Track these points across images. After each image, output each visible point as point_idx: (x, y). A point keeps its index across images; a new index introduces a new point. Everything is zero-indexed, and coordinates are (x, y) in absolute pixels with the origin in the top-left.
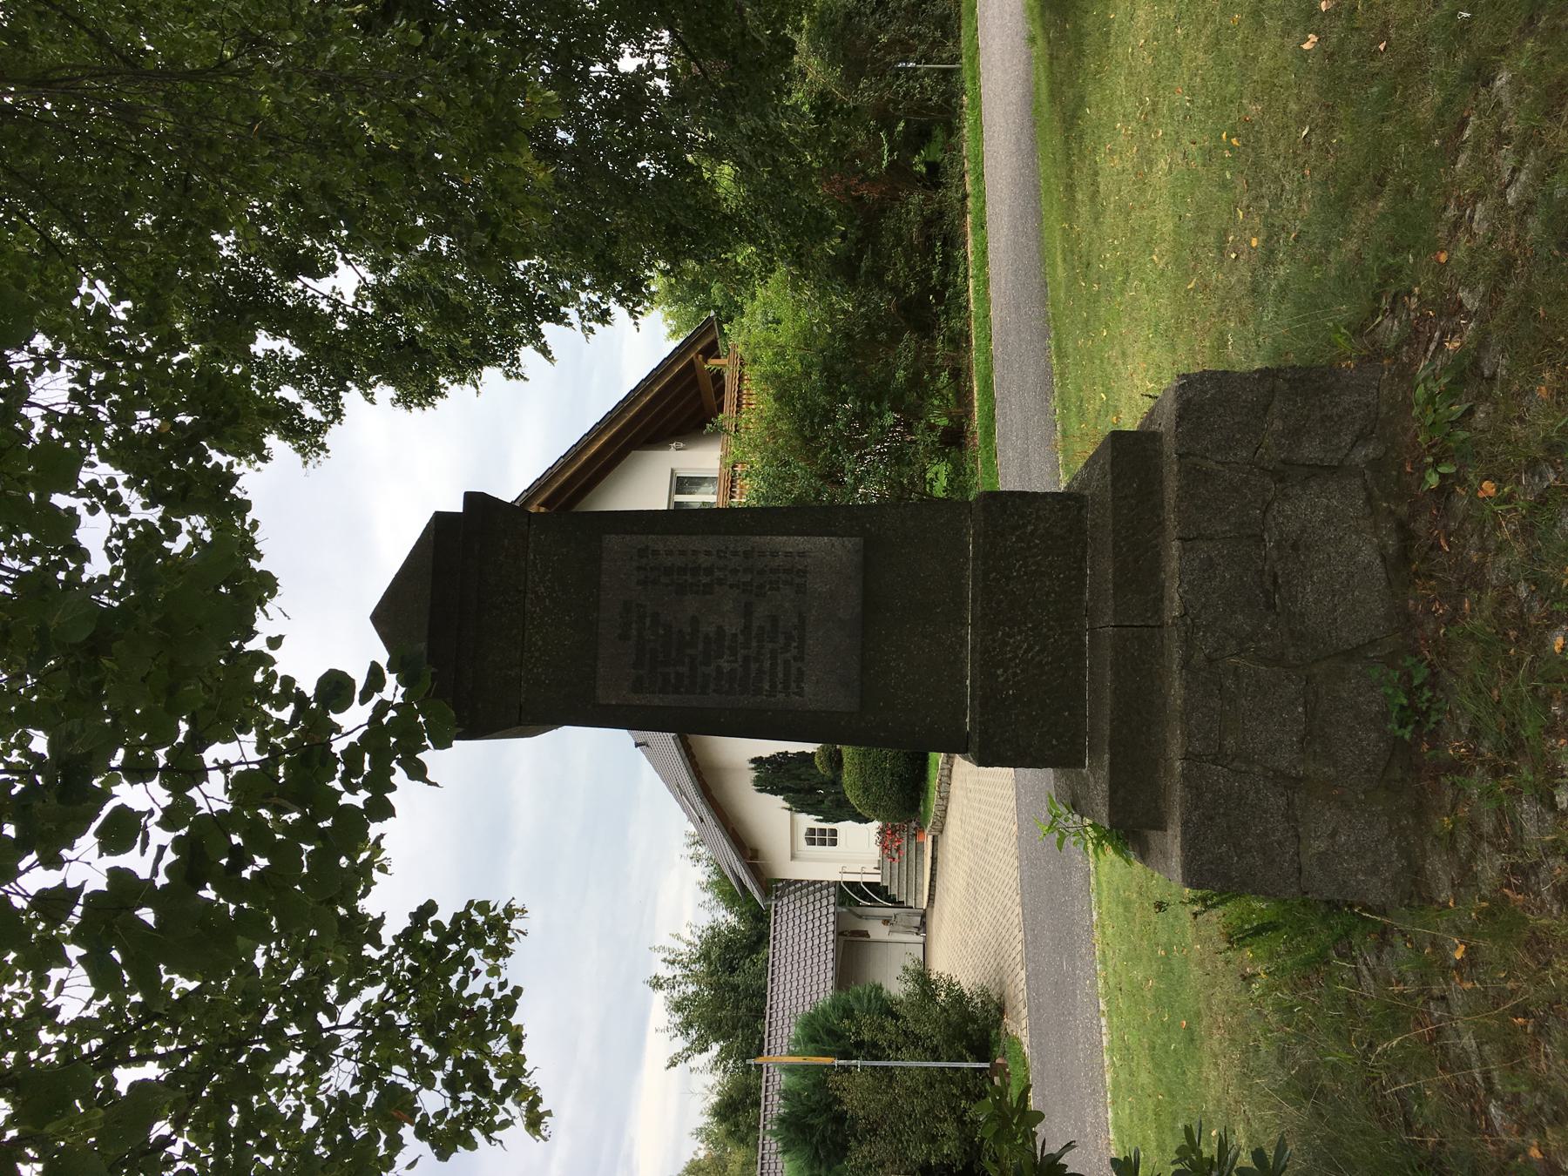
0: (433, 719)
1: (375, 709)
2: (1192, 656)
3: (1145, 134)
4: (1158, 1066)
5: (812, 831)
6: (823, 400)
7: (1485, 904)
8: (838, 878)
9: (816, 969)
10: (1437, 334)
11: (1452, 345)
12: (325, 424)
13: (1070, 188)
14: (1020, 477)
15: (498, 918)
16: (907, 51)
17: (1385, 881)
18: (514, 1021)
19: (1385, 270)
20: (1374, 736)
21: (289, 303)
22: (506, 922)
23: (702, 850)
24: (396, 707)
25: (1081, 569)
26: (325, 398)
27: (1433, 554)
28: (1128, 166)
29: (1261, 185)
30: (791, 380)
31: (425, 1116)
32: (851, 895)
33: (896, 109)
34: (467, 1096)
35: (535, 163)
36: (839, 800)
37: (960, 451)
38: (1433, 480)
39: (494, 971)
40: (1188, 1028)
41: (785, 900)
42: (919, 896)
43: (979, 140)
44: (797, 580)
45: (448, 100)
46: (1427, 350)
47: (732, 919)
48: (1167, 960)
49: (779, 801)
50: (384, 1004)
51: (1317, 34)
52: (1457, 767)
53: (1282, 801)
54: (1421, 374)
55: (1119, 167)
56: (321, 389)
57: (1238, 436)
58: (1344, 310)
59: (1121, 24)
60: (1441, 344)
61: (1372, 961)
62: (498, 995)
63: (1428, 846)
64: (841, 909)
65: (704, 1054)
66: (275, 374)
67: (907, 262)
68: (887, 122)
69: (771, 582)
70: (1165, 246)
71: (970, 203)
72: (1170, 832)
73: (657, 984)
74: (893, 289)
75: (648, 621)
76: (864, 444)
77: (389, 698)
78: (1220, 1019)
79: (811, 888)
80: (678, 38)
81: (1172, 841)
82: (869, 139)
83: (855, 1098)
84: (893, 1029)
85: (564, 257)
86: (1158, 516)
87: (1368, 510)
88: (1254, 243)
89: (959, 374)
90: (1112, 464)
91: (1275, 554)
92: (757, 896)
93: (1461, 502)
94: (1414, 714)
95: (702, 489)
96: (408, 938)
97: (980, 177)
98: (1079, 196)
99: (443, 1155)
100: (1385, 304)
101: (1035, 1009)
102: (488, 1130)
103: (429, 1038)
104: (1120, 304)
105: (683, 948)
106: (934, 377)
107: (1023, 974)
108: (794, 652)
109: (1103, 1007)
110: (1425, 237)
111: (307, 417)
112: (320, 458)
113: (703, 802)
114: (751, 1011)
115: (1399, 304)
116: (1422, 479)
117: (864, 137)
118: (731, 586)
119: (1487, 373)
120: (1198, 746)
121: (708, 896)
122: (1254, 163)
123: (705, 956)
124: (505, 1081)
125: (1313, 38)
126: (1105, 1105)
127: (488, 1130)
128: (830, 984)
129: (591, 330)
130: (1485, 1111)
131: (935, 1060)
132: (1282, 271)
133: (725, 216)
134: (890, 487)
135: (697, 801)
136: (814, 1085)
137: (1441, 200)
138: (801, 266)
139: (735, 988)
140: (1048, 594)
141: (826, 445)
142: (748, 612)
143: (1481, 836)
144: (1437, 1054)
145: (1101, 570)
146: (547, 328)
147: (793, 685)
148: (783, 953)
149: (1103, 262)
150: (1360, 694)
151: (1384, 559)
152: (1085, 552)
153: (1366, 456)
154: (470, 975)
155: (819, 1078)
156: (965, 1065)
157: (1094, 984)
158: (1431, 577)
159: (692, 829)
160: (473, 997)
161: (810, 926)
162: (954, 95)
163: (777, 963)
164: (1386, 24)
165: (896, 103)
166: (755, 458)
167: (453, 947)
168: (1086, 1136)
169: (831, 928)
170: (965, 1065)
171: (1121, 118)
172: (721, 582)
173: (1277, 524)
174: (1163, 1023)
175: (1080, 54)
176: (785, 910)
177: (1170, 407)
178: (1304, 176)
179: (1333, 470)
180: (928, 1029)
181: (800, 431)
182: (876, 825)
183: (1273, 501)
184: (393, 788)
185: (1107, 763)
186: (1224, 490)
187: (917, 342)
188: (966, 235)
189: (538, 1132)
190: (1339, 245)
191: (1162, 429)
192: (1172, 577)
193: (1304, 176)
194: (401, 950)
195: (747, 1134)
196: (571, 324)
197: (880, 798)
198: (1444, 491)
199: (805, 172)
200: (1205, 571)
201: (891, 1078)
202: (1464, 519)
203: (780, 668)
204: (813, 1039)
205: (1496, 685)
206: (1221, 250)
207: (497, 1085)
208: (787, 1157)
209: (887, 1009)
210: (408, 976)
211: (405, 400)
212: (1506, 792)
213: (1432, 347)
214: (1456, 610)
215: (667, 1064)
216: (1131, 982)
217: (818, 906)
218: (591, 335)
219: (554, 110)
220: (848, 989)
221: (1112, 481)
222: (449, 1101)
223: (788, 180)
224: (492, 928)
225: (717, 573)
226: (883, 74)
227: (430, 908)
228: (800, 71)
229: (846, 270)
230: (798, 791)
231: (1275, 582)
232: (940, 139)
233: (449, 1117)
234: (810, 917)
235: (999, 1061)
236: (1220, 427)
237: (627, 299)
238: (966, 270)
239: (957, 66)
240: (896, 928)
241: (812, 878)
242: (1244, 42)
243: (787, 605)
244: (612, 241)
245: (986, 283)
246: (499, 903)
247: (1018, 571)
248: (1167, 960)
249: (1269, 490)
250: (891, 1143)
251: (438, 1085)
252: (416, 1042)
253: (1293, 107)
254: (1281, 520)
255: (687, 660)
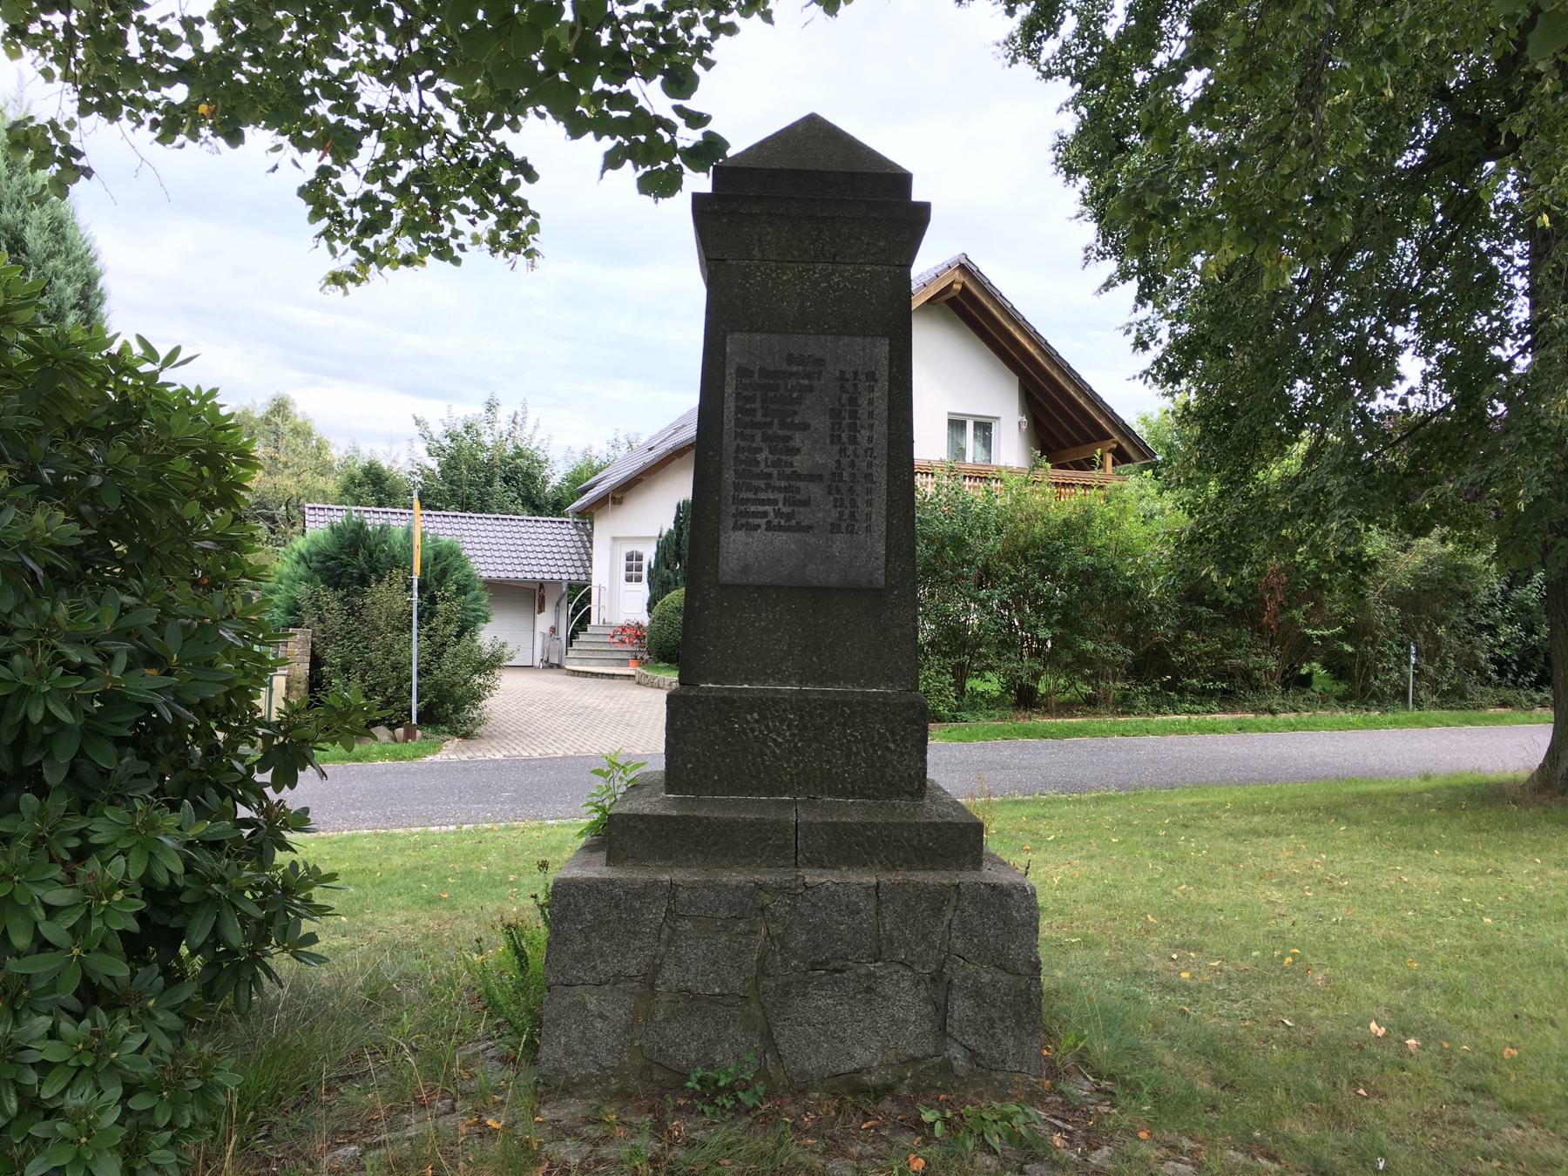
0: (665, 176)
1: (668, 121)
2: (766, 892)
3: (1311, 881)
4: (407, 872)
5: (640, 558)
6: (1064, 567)
7: (535, 1146)
8: (595, 583)
9: (507, 561)
10: (1070, 1127)
11: (1057, 1139)
12: (1037, 63)
13: (1266, 811)
14: (982, 761)
15: (525, 243)
16: (1429, 655)
17: (560, 1062)
18: (430, 259)
19: (1139, 1086)
20: (693, 1056)
21: (1164, 23)
22: (523, 251)
23: (624, 450)
24: (673, 142)
25: (853, 794)
26: (1063, 62)
27: (859, 1114)
28: (1281, 864)
29: (1242, 982)
30: (1084, 535)
31: (337, 175)
32: (579, 597)
33: (1366, 644)
34: (358, 214)
35: (1225, 262)
36: (669, 583)
37: (1013, 705)
38: (928, 1117)
39: (476, 239)
40: (441, 899)
41: (574, 532)
42: (577, 662)
43: (1331, 727)
44: (844, 525)
45: (1289, 177)
46: (1055, 1117)
47: (555, 481)
48: (504, 882)
49: (669, 524)
50: (442, 134)
51: (1385, 1036)
52: (659, 1128)
53: (632, 971)
54: (1031, 1111)
55: (1281, 856)
56: (1073, 57)
57: (976, 941)
58: (1101, 1048)
59: (1428, 860)
60: (1060, 1129)
61: (490, 1053)
62: (453, 243)
63: (590, 1102)
64: (565, 585)
65: (426, 453)
66: (1088, 11)
67: (1206, 653)
68: (1351, 634)
69: (842, 499)
70: (1194, 896)
71: (1267, 717)
72: (605, 869)
73: (491, 407)
74: (1178, 638)
75: (806, 382)
76: (1020, 610)
77: (679, 133)
78: (448, 926)
79: (585, 557)
80: (1432, 417)
81: (598, 870)
82: (1335, 616)
83: (387, 598)
84: (447, 632)
85: (1201, 302)
86: (901, 866)
87: (904, 1058)
88: (1185, 975)
89: (1091, 704)
90: (950, 823)
91: (863, 971)
92: (578, 503)
93: (904, 1139)
94: (710, 1092)
95: (980, 448)
96: (503, 156)
97: (1292, 727)
98: (1257, 819)
99: (303, 192)
100: (1104, 1084)
101: (466, 767)
102: (327, 234)
103: (413, 177)
104: (1141, 854)
105: (528, 431)
106: (1087, 680)
107: (499, 756)
108: (775, 522)
109: (465, 827)
110: (1165, 1121)
111: (1044, 44)
112: (1003, 59)
113: (667, 450)
114: (468, 498)
115: (1103, 1096)
116: (930, 1107)
117: (1337, 611)
118: (838, 462)
119: (1027, 1167)
120: (684, 895)
121: (579, 457)
122: (1264, 977)
123: (519, 454)
124: (372, 250)
125: (1381, 1032)
126: (375, 828)
127: (327, 234)
128: (494, 575)
129: (1128, 332)
130: (351, 1142)
131: (418, 672)
132: (1152, 999)
133: (1247, 468)
134: (975, 635)
135: (669, 445)
136: (394, 557)
137: (1200, 1136)
138: (1190, 542)
139: (489, 482)
140: (829, 762)
141: (1018, 571)
142: (814, 478)
143: (597, 1145)
144: (404, 1103)
145: (851, 811)
146: (1133, 286)
147: (743, 521)
148: (523, 530)
149: (1187, 840)
150: (731, 1045)
151: (857, 1071)
152: (869, 798)
153: (956, 1058)
154: (471, 217)
155: (400, 562)
156: (414, 700)
157: (487, 820)
158: (838, 1111)
159: (644, 439)
160: (450, 219)
161: (549, 556)
162: (1380, 703)
163: (513, 523)
164: (1384, 1096)
165: (1372, 644)
166: (1003, 501)
167: (497, 199)
168: (347, 810)
169: (547, 576)
170: (414, 700)
171: (1331, 858)
172: (842, 451)
173: (891, 974)
174: (446, 877)
175: (1403, 822)
176: (564, 532)
177: (1005, 878)
178: (1244, 1020)
179: (943, 1027)
180: (448, 666)
181: (1034, 545)
182: (645, 619)
183: (913, 970)
184: (598, 138)
185: (669, 813)
186: (924, 926)
187: (1123, 662)
188: (1233, 712)
189: (328, 283)
190: (1171, 1048)
191: (985, 871)
192: (842, 876)
193: (1244, 1020)
194: (493, 149)
195: (352, 495)
196: (1135, 311)
197: (671, 624)
198: (919, 1126)
199: (1288, 547)
200: (847, 907)
201: (402, 630)
202: (890, 1142)
203: (760, 509)
204: (437, 556)
205: (734, 1163)
206: (1182, 946)
207: (368, 243)
208: (327, 530)
209: (466, 628)
210: (469, 157)
211: (1061, 144)
212: (636, 1168)
213: (1058, 1123)
214: (806, 1132)
215: (418, 416)
216: (485, 851)
217: (568, 563)
218: (1123, 332)
219: (1271, 282)
220: (485, 589)
221: (935, 823)
222: (352, 197)
223: (1280, 527)
224: (516, 237)
225: (850, 448)
226: (1405, 631)
227: (531, 176)
228: (1408, 546)
229: (1195, 593)
230: (678, 544)
231: (836, 970)
232: (1335, 688)
233: (338, 197)
234: (557, 556)
235: (419, 733)
236: (984, 924)
237: (1160, 368)
238: (1197, 713)
239: (1411, 706)
240: (547, 639)
241: (595, 557)
242: (1388, 971)
243: (820, 515)
244: (1221, 352)
245: (1182, 732)
246: (536, 242)
247: (851, 735)
248: (504, 882)
249: (923, 968)
250: (341, 629)
251: (367, 187)
252: (408, 166)
253: (1316, 1012)
254: (895, 977)
255: (768, 419)
